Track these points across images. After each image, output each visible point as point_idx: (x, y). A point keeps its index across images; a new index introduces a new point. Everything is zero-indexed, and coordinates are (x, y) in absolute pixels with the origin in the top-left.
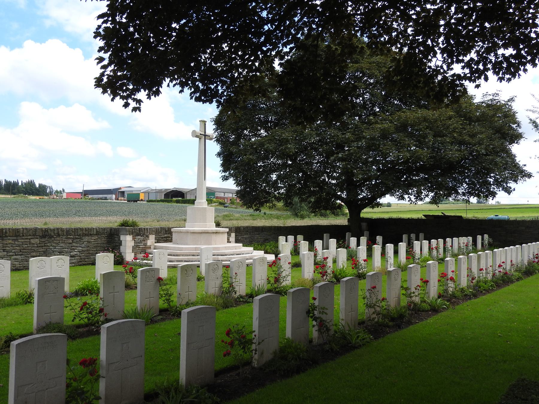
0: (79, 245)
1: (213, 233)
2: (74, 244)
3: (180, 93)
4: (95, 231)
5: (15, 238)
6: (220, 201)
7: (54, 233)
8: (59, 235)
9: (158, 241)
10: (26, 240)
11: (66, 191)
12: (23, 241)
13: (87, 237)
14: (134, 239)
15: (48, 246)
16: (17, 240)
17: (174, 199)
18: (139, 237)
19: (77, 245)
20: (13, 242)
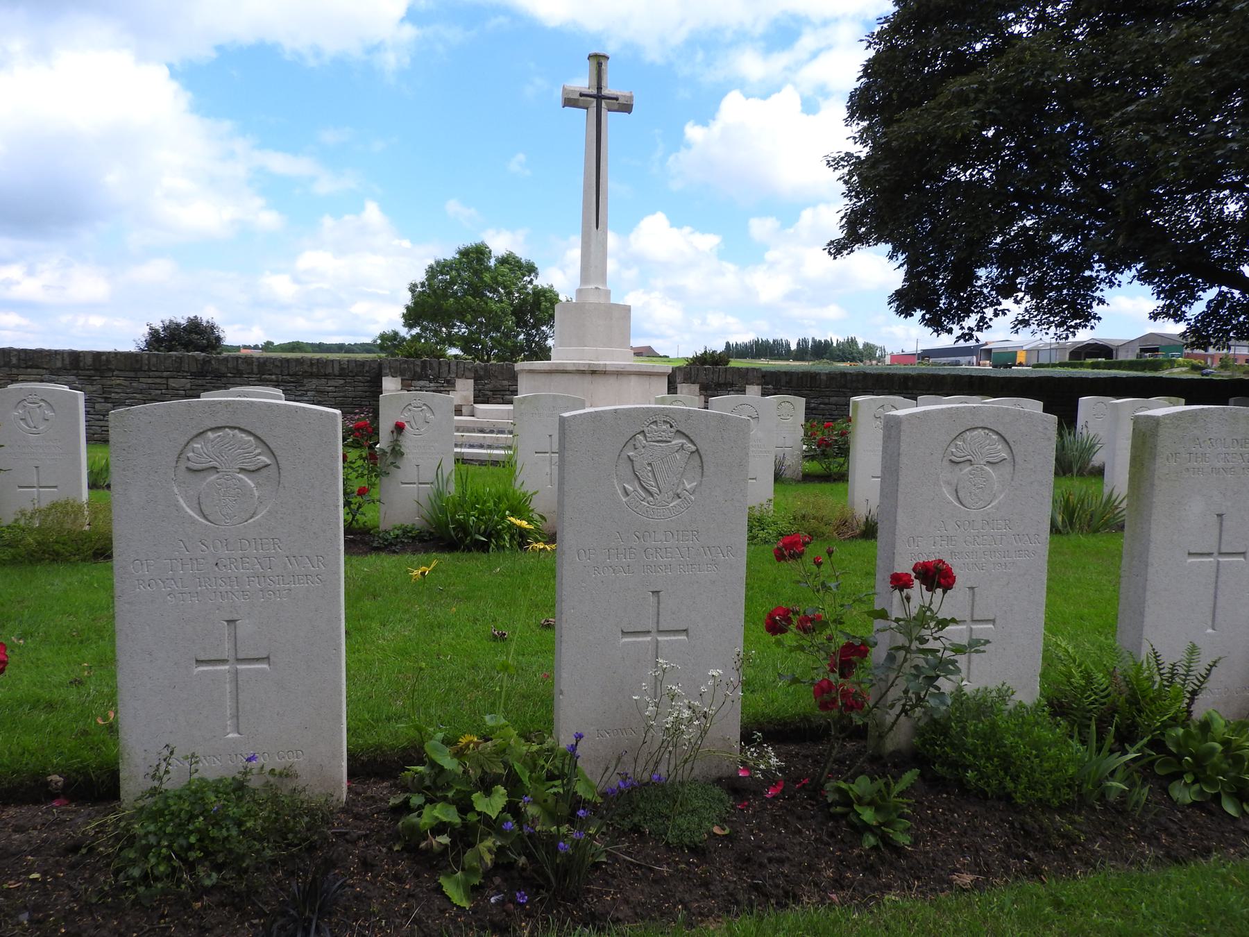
1: (582, 372)
5: (132, 374)
6: (1195, 362)
9: (480, 398)
10: (158, 380)
11: (889, 351)
12: (150, 381)
13: (315, 381)
16: (136, 379)
17: (1089, 361)
20: (127, 383)
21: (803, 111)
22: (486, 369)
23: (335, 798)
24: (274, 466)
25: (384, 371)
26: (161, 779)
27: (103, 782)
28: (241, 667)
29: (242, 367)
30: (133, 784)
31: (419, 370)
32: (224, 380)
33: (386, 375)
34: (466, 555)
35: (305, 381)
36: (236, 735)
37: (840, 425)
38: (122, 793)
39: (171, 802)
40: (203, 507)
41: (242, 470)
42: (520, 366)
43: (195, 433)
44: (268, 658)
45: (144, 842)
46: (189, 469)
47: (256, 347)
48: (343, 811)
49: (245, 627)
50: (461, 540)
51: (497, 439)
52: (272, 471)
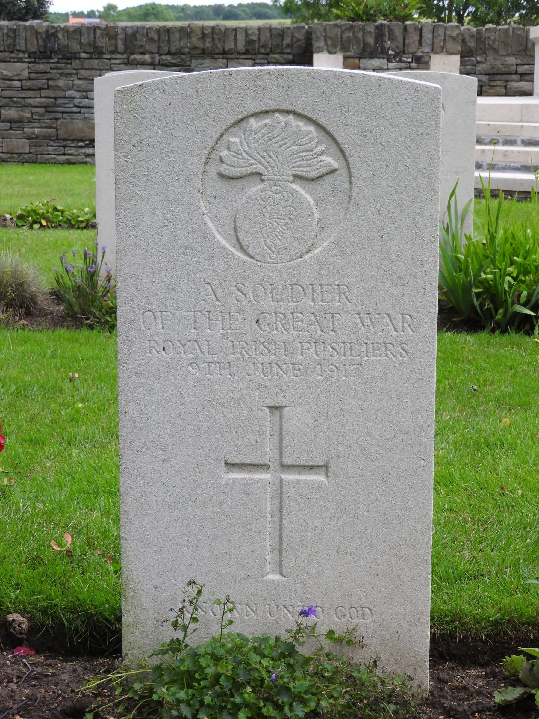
3: (218, 173)
4: (241, 38)
7: (81, 43)
15: (58, 88)
22: (479, 37)
23: (415, 683)
24: (343, 172)
25: (316, 44)
26: (185, 628)
27: (77, 630)
28: (288, 477)
29: (102, 42)
30: (143, 635)
31: (371, 40)
32: (76, 63)
33: (320, 51)
34: (497, 338)
36: (278, 577)
38: (124, 644)
39: (203, 662)
40: (241, 234)
41: (298, 178)
43: (232, 119)
44: (326, 466)
45: (174, 713)
46: (221, 175)
47: (91, 14)
48: (426, 702)
49: (295, 418)
50: (490, 315)
51: (505, 154)
52: (340, 180)
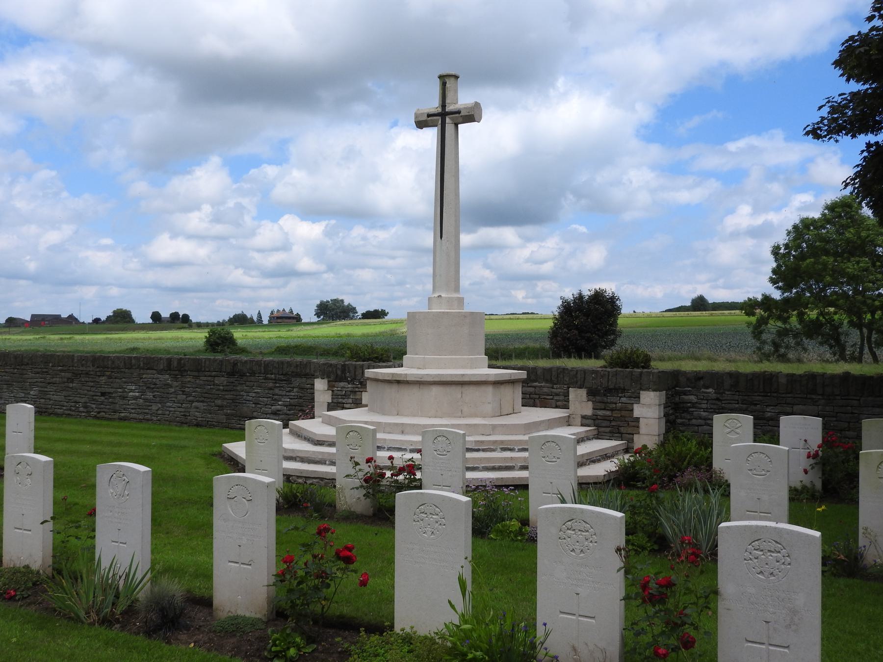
0: (284, 393)
2: (277, 391)
5: (196, 374)
8: (253, 373)
12: (205, 378)
13: (298, 380)
14: (330, 387)
15: (237, 390)
18: (342, 384)
19: (280, 393)
20: (193, 380)
21: (837, 63)
31: (339, 372)
35: (293, 379)
37: (61, 495)
42: (370, 373)
